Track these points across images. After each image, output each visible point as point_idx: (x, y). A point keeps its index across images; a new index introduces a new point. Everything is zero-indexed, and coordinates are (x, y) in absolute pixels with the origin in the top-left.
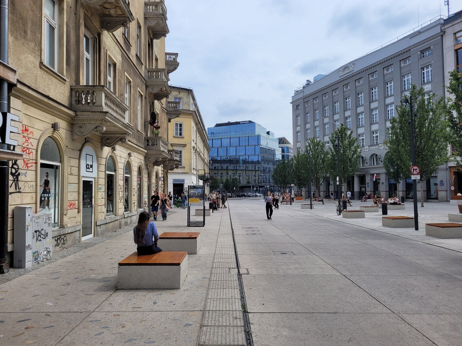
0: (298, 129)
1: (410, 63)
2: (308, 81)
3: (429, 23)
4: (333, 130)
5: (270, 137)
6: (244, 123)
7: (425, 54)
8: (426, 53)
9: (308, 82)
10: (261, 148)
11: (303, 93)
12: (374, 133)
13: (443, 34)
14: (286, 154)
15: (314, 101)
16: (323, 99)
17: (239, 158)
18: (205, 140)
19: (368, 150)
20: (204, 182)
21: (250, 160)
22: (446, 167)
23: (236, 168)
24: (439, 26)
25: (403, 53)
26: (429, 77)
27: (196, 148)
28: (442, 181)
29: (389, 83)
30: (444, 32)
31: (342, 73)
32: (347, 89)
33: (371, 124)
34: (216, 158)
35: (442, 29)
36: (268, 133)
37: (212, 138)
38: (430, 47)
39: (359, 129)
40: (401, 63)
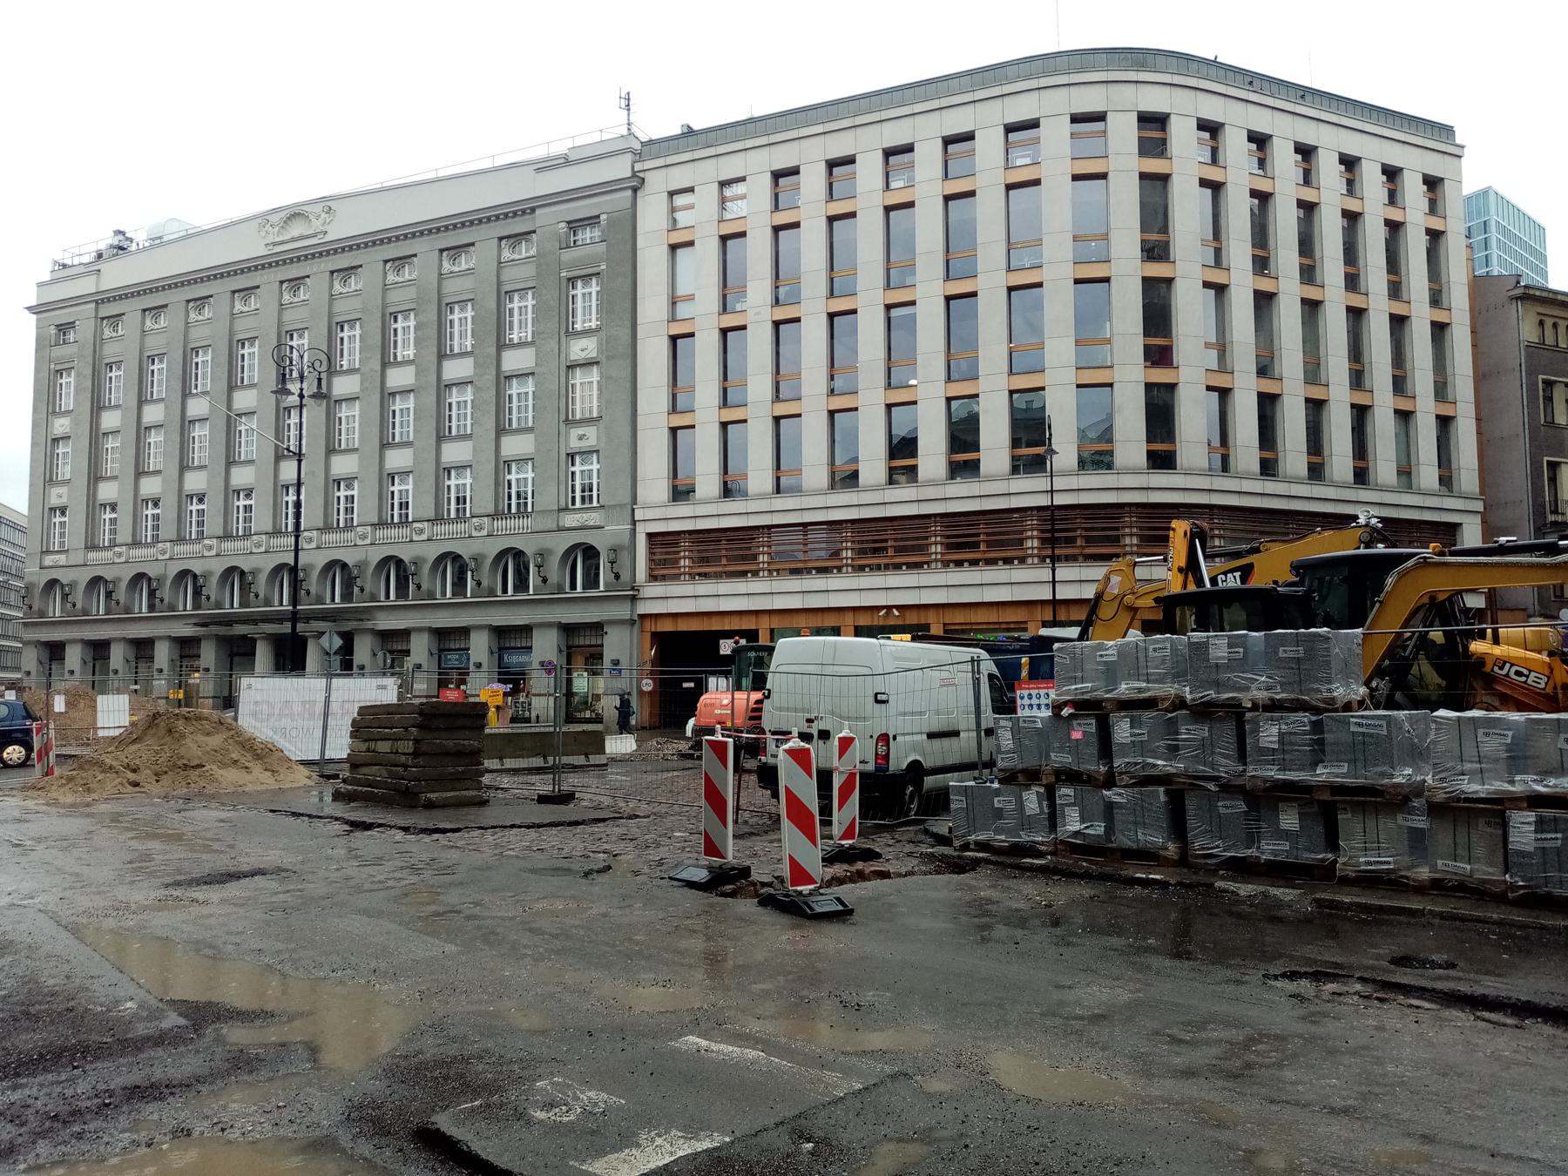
1: (414, 277)
3: (596, 138)
4: (381, 432)
12: (393, 478)
13: (636, 185)
16: (235, 311)
22: (631, 615)
25: (511, 215)
28: (616, 663)
30: (640, 181)
31: (279, 232)
32: (296, 300)
35: (638, 167)
38: (598, 216)
40: (503, 246)
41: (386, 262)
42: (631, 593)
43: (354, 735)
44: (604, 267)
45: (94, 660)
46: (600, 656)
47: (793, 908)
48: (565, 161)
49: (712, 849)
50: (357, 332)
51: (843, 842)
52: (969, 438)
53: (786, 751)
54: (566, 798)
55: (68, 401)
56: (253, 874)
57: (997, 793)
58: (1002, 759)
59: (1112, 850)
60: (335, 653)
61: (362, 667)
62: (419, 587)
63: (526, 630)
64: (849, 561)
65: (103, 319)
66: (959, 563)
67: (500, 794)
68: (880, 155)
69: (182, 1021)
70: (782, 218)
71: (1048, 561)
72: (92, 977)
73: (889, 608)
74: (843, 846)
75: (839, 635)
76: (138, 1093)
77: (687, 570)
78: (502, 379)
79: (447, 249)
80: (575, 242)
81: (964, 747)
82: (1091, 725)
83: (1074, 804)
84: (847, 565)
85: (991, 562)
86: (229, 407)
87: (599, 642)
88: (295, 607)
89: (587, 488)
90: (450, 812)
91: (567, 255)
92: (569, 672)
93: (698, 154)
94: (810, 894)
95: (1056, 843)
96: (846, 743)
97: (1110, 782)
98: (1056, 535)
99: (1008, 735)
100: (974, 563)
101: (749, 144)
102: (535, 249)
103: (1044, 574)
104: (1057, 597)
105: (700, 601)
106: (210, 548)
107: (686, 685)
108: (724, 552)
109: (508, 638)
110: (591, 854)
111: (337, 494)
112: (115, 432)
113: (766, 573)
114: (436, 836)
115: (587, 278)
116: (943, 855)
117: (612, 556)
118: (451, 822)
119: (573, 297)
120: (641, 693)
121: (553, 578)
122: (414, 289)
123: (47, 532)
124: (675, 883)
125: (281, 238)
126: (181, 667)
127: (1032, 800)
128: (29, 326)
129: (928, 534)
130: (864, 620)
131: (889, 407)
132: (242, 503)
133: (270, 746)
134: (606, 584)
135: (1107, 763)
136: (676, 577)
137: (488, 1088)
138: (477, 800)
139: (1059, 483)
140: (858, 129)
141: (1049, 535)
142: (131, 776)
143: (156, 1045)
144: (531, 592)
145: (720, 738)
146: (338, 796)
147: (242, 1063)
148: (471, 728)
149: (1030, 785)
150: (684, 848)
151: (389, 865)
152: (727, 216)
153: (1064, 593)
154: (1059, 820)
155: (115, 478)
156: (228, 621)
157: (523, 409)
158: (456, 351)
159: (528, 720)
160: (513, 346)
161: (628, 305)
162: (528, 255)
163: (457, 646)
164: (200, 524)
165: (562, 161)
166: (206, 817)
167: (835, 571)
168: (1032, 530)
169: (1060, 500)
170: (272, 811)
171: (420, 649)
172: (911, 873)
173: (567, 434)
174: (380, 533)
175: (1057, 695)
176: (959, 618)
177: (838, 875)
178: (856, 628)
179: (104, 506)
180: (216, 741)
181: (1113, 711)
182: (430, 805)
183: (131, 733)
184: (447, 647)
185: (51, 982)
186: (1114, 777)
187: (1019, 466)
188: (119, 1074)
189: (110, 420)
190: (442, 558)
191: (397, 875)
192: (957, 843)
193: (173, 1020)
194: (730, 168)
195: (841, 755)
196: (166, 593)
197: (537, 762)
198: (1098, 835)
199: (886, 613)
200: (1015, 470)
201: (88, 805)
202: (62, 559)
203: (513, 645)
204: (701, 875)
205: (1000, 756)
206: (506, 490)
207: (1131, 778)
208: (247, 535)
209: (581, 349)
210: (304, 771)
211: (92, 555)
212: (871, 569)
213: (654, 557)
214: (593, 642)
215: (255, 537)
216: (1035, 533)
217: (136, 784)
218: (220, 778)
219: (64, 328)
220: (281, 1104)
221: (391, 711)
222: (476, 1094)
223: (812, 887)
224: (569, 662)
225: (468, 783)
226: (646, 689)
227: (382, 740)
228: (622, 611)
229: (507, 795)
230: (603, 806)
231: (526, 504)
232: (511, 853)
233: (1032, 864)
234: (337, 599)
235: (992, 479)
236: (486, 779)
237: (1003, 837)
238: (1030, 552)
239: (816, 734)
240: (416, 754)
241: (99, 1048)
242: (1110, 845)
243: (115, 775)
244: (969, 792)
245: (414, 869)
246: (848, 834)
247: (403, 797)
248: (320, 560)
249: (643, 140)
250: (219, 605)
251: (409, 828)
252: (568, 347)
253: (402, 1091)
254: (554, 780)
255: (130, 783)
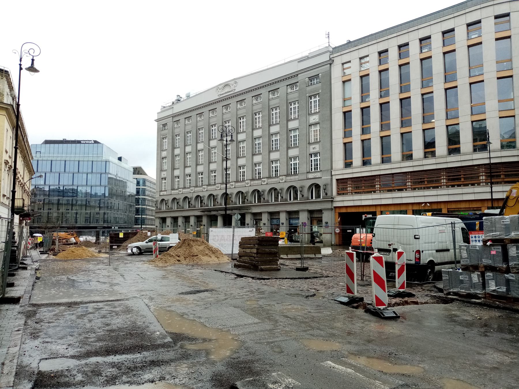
0: (164, 154)
2: (178, 96)
5: (122, 164)
6: (87, 143)
7: (313, 82)
8: (314, 80)
9: (179, 97)
10: (109, 178)
11: (173, 110)
12: (256, 165)
13: (331, 62)
14: (141, 187)
15: (186, 122)
17: (77, 190)
18: (27, 156)
19: (249, 185)
20: (21, 219)
21: (93, 193)
23: (72, 202)
24: (328, 54)
26: (316, 107)
27: (10, 164)
28: (327, 223)
29: (293, 104)
33: (253, 155)
34: (41, 187)
35: (331, 56)
36: (120, 159)
37: (37, 159)
38: (319, 74)
39: (239, 160)
41: (253, 97)
42: (331, 199)
43: (240, 246)
44: (321, 91)
45: (174, 222)
46: (321, 221)
47: (377, 314)
48: (307, 58)
49: (349, 290)
50: (245, 120)
51: (400, 290)
52: (456, 140)
53: (373, 257)
54: (305, 269)
55: (166, 147)
56: (204, 291)
57: (461, 274)
58: (463, 261)
59: (509, 298)
60: (239, 220)
61: (248, 224)
62: (264, 199)
63: (297, 212)
64: (410, 186)
65: (174, 122)
66: (453, 186)
67: (285, 267)
68: (418, 41)
69: (171, 340)
70: (382, 67)
71: (489, 184)
72: (150, 323)
73: (426, 203)
74: (400, 291)
75: (407, 214)
76: (154, 363)
77: (350, 191)
78: (289, 131)
79: (271, 91)
80: (311, 84)
81: (448, 256)
82: (499, 249)
83: (493, 279)
84: (409, 188)
85: (465, 185)
86: (209, 146)
87: (321, 216)
88: (226, 206)
89: (316, 165)
90: (268, 272)
91: (309, 89)
92: (311, 227)
93: (352, 50)
94: (384, 309)
95: (485, 294)
96: (400, 254)
97: (508, 271)
98: (492, 174)
99: (465, 252)
100: (459, 186)
101: (370, 43)
102: (298, 88)
103: (488, 189)
104: (493, 198)
105: (355, 202)
106: (205, 188)
107: (348, 231)
108: (363, 185)
109: (292, 215)
110: (310, 290)
111: (240, 171)
112: (178, 155)
113: (379, 192)
114: (261, 281)
115: (315, 96)
116: (440, 297)
117: (324, 187)
118: (267, 276)
119: (311, 102)
120: (335, 233)
121: (305, 195)
122: (261, 104)
123: (161, 184)
124: (336, 302)
125: (222, 93)
126: (197, 224)
127: (475, 277)
128: (155, 126)
129: (347, 184)
130: (416, 208)
131: (424, 130)
132: (213, 174)
133: (217, 249)
134: (323, 197)
135: (506, 264)
136: (347, 194)
137: (258, 374)
138: (276, 269)
139: (492, 155)
140: (409, 33)
141: (489, 174)
142: (178, 258)
143: (162, 347)
144: (299, 200)
145: (351, 252)
146: (236, 266)
147: (185, 356)
148: (274, 245)
149: (474, 271)
150: (342, 289)
151: (245, 290)
152: (362, 69)
153: (495, 196)
154: (486, 285)
155: (190, 166)
156: (210, 210)
157: (295, 140)
158: (274, 123)
159: (298, 242)
160: (291, 120)
161: (329, 103)
162: (296, 90)
163: (276, 218)
164: (202, 181)
165: (307, 58)
166: (197, 271)
167: (404, 190)
168: (482, 173)
169: (493, 161)
170: (215, 270)
171: (265, 218)
172: (426, 303)
173: (309, 147)
174: (252, 182)
175: (485, 237)
176: (453, 206)
177: (397, 302)
178: (413, 211)
179: (176, 177)
180: (201, 248)
181: (508, 244)
182: (262, 270)
183: (178, 245)
184: (273, 218)
185: (139, 324)
186: (510, 269)
187: (383, 161)
188: (148, 355)
189: (177, 151)
190: (271, 190)
191: (247, 294)
192: (445, 292)
193: (169, 339)
194: (363, 53)
195: (398, 258)
196: (193, 202)
197: (299, 256)
198: (503, 292)
199: (425, 205)
200: (475, 150)
201: (166, 267)
202: (165, 193)
203: (293, 217)
204: (345, 300)
205: (462, 260)
206: (290, 167)
207: (517, 270)
208: (215, 184)
209: (314, 119)
210: (226, 256)
211: (173, 192)
212: (418, 189)
213: (338, 187)
214: (319, 216)
215: (217, 185)
216: (484, 174)
217: (179, 261)
218: (203, 259)
219: (164, 125)
220: (193, 372)
221: (250, 239)
222: (253, 375)
223: (384, 307)
224: (311, 224)
225: (273, 263)
226: (337, 232)
227: (248, 248)
228: (328, 206)
229: (287, 267)
230: (317, 272)
231: (296, 171)
232: (284, 288)
233: (475, 302)
234: (241, 203)
235: (465, 154)
236: (280, 261)
237: (464, 291)
238: (481, 181)
239: (392, 250)
240: (257, 253)
241: (146, 347)
242: (508, 296)
243: (173, 258)
244: (450, 273)
245: (252, 292)
246: (402, 287)
247: (254, 267)
248: (235, 191)
249: (333, 47)
250: (207, 206)
251: (254, 277)
252: (309, 119)
253: (231, 371)
254: (301, 263)
255: (178, 260)
